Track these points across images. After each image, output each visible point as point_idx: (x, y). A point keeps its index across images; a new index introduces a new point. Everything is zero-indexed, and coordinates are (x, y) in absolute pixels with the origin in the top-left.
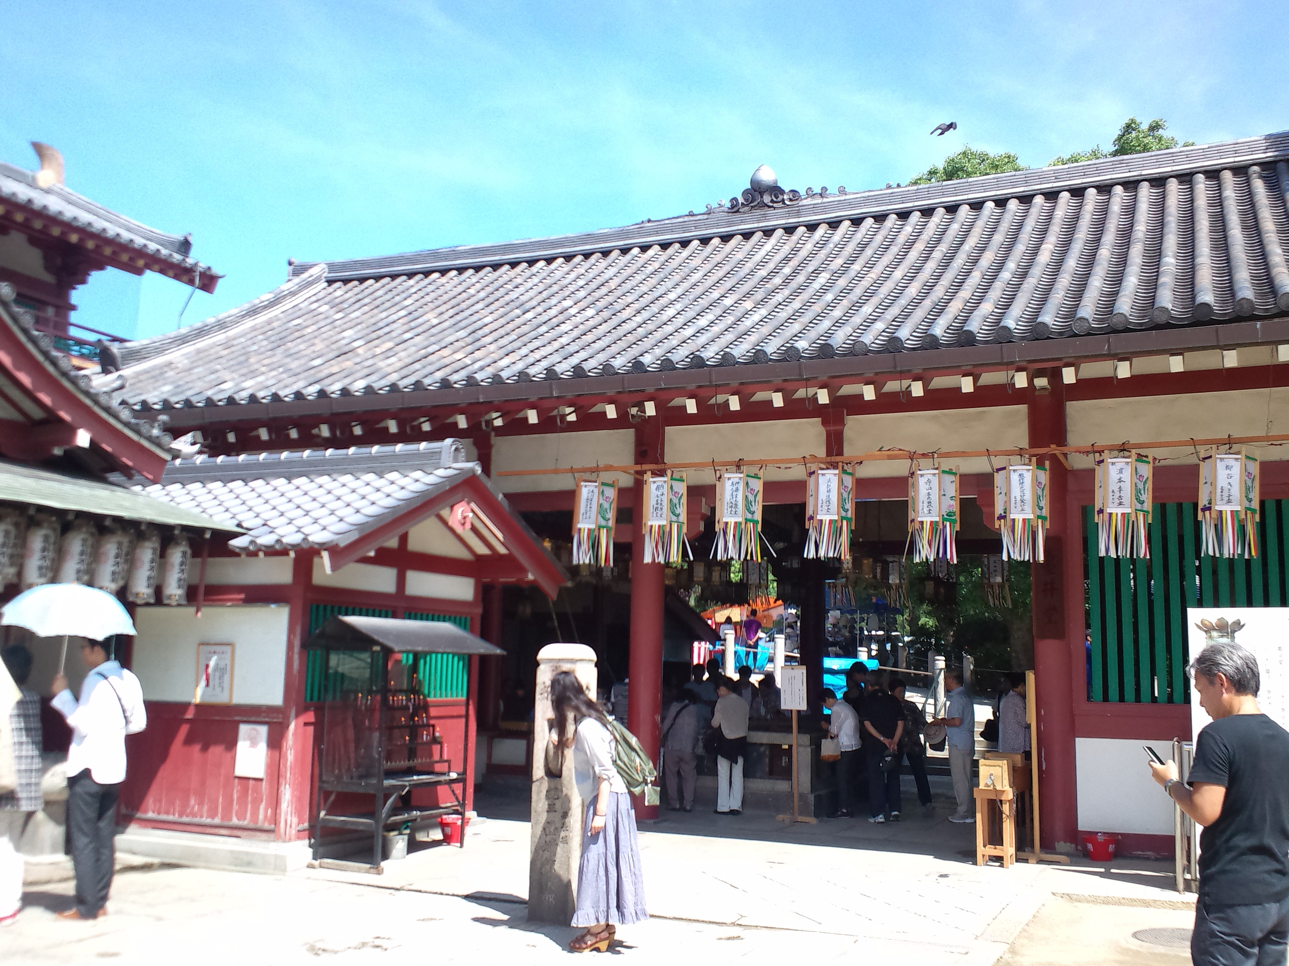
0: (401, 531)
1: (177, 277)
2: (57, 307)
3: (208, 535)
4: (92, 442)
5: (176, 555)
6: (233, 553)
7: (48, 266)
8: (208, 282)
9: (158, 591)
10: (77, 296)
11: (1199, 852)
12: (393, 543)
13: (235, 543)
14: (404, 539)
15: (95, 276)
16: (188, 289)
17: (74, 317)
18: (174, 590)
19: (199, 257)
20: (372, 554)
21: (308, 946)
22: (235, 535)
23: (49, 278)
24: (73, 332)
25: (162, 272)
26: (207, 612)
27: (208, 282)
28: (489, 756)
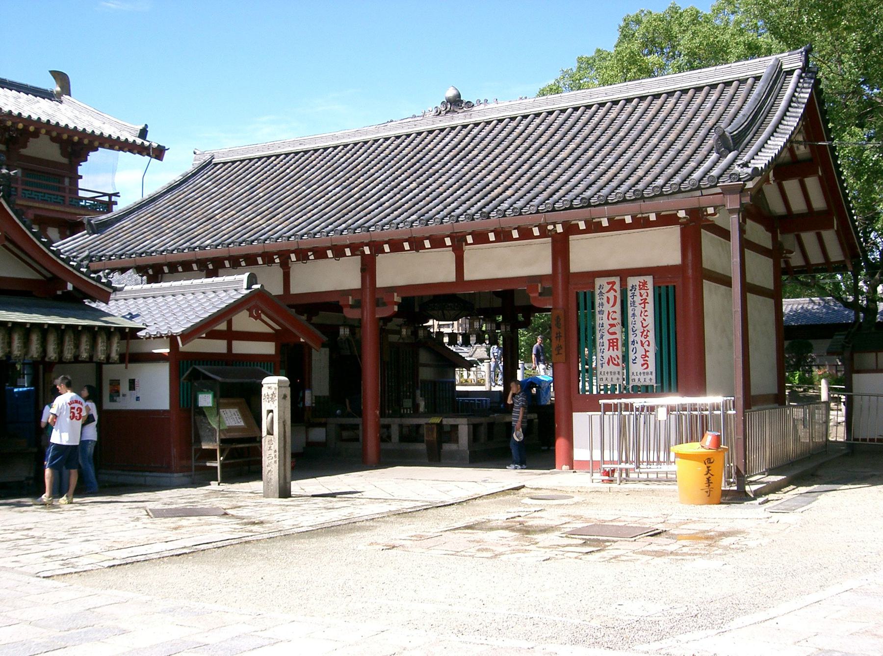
0: (229, 318)
1: (140, 153)
2: (70, 178)
3: (127, 330)
4: (74, 287)
5: (115, 340)
6: (138, 338)
7: (64, 153)
8: (159, 153)
9: (108, 357)
10: (82, 169)
11: (816, 486)
12: (222, 326)
13: (139, 334)
14: (230, 323)
15: (92, 156)
16: (147, 158)
17: (81, 184)
18: (114, 356)
19: (153, 139)
20: (204, 335)
21: (52, 424)
22: (141, 329)
23: (65, 160)
24: (81, 194)
25: (131, 151)
26: (132, 366)
27: (159, 153)
28: (307, 438)
